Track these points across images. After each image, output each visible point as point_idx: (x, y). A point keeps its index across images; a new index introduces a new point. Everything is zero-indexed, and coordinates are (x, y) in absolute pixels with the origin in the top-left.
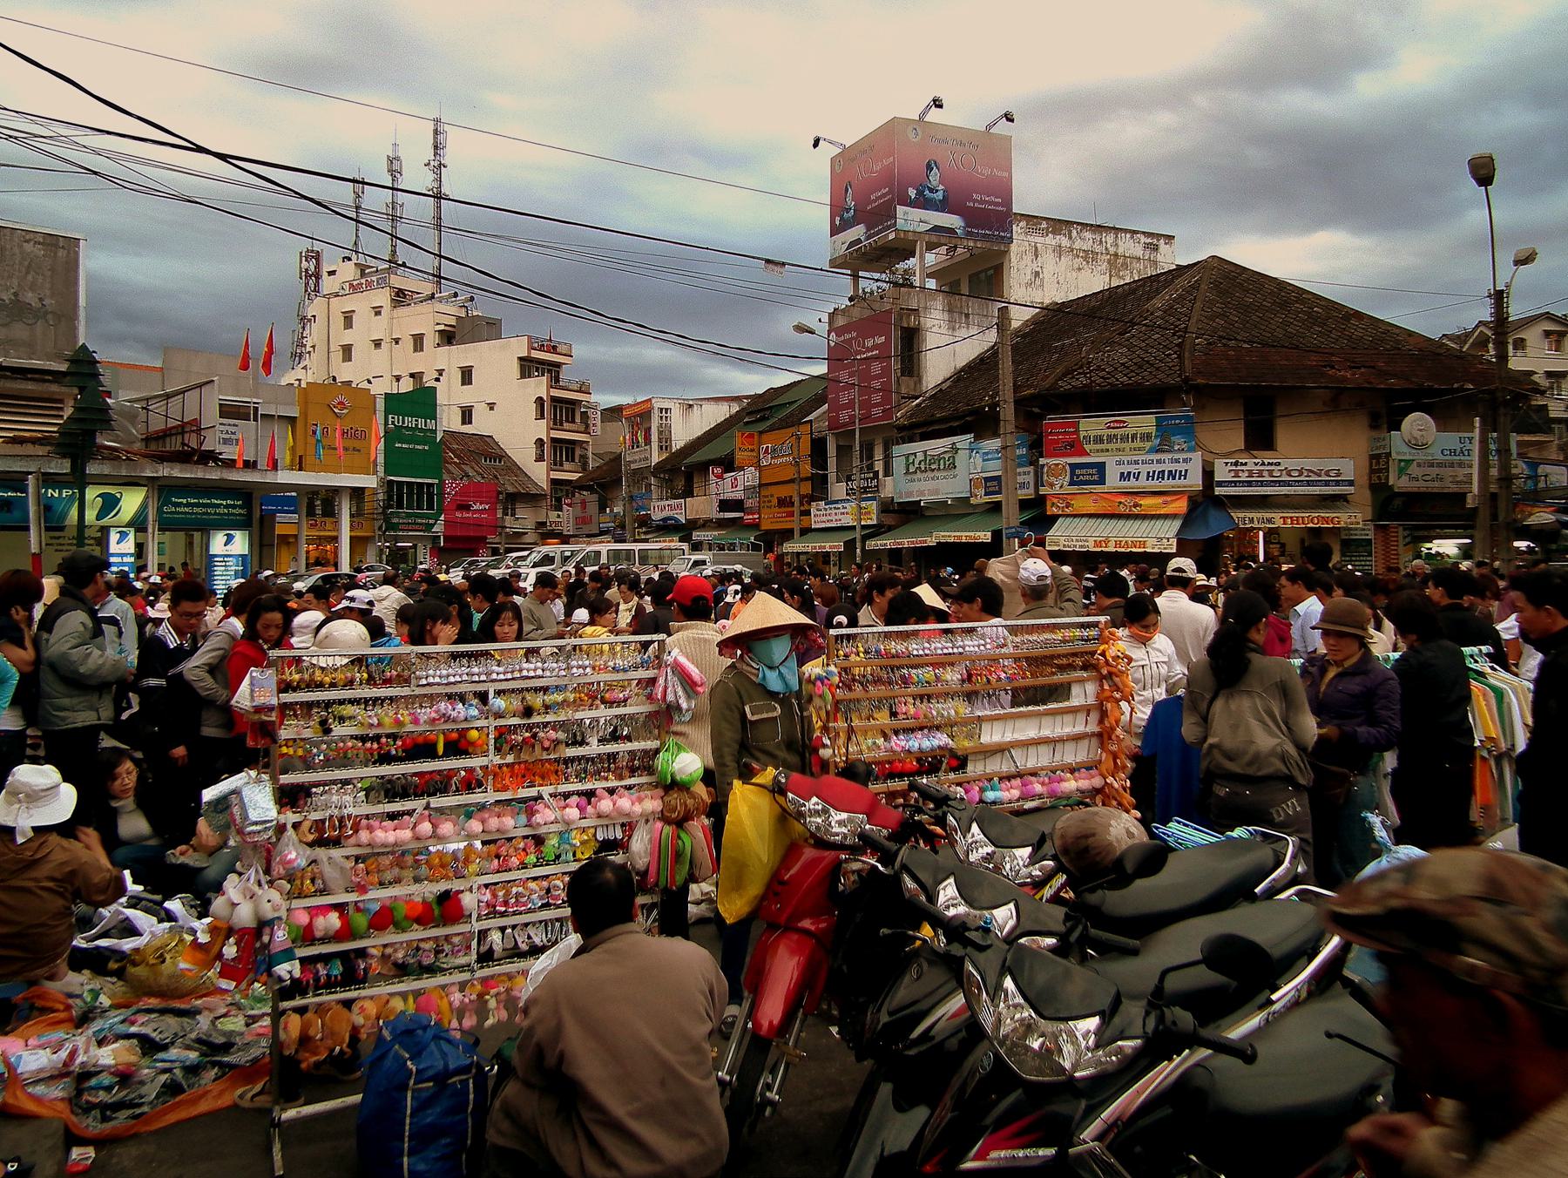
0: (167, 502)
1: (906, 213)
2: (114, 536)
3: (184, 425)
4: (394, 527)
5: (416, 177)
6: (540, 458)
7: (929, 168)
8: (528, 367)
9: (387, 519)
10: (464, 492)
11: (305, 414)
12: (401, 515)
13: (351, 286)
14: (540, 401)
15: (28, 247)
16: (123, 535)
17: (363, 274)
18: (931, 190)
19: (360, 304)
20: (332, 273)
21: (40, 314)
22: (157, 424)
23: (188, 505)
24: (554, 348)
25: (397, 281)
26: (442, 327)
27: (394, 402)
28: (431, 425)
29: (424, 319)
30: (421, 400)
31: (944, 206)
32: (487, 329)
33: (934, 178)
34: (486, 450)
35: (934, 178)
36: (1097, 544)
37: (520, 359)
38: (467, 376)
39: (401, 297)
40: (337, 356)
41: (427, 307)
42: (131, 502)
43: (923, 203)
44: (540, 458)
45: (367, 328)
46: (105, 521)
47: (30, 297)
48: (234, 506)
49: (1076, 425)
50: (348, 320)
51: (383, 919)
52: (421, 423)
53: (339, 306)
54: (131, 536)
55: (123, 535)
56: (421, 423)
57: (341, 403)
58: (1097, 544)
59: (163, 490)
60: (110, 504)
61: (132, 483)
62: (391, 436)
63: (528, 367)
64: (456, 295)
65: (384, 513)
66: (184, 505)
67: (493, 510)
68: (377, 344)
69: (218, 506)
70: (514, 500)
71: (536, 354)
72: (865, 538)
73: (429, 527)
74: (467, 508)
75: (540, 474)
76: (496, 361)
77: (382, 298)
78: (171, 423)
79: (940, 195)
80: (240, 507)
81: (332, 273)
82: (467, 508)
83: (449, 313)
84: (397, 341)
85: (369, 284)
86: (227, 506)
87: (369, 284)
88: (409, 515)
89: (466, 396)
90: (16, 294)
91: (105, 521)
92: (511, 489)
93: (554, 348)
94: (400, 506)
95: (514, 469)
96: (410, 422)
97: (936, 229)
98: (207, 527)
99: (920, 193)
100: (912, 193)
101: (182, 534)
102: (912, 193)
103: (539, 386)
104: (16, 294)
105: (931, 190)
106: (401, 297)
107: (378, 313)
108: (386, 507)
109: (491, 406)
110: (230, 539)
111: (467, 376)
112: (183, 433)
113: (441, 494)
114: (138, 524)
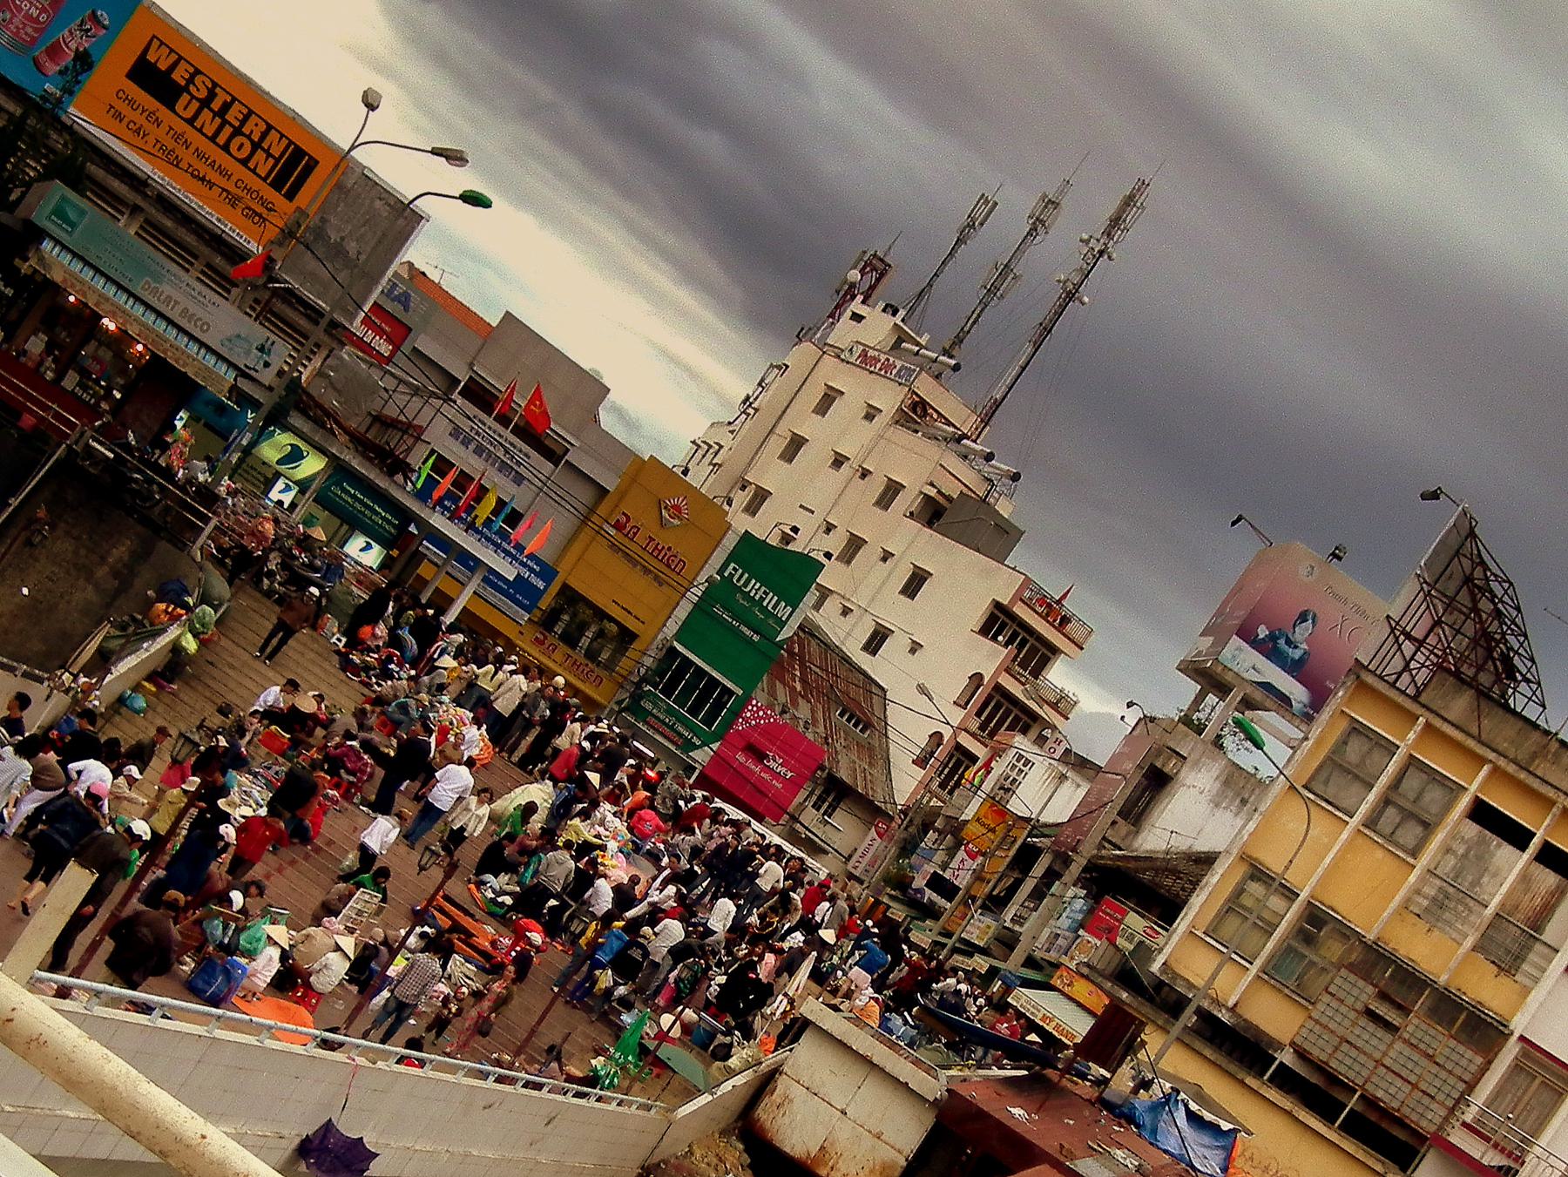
0: (339, 484)
1: (1239, 649)
2: (280, 485)
3: (410, 425)
4: (642, 714)
5: (1056, 256)
6: (921, 762)
7: (1303, 617)
8: (998, 622)
9: (637, 697)
10: (771, 732)
11: (622, 493)
12: (660, 704)
13: (864, 354)
14: (977, 679)
15: (378, 204)
16: (287, 488)
17: (896, 346)
18: (1289, 642)
19: (857, 388)
20: (857, 318)
21: (350, 264)
22: (391, 411)
23: (353, 496)
24: (1065, 620)
25: (926, 387)
26: (932, 492)
27: (750, 550)
28: (783, 611)
29: (918, 465)
30: (791, 572)
31: (1295, 668)
32: (994, 538)
33: (1302, 633)
34: (861, 706)
35: (1302, 633)
36: (1044, 1018)
37: (997, 605)
38: (915, 582)
39: (916, 414)
40: (778, 444)
41: (933, 451)
42: (312, 465)
43: (1269, 649)
44: (921, 762)
45: (840, 430)
46: (282, 468)
47: (352, 247)
48: (389, 522)
49: (1124, 913)
50: (829, 398)
51: (233, 531)
52: (770, 601)
53: (832, 373)
54: (292, 494)
55: (287, 488)
56: (770, 601)
57: (677, 508)
58: (1044, 1018)
59: (338, 470)
60: (295, 456)
61: (322, 451)
62: (720, 591)
63: (998, 622)
64: (989, 457)
65: (638, 685)
66: (349, 494)
67: (794, 785)
68: (839, 461)
69: (378, 514)
70: (836, 793)
71: (1020, 610)
72: (955, 950)
73: (689, 746)
74: (760, 756)
75: (906, 782)
76: (969, 582)
77: (889, 398)
78: (402, 418)
79: (1297, 654)
80: (394, 526)
81: (857, 318)
82: (760, 756)
83: (960, 477)
84: (865, 474)
85: (888, 367)
86: (383, 518)
87: (888, 367)
88: (670, 711)
89: (895, 612)
90: (342, 239)
91: (282, 468)
92: (844, 774)
93: (1065, 620)
94: (668, 692)
95: (878, 756)
96: (754, 588)
97: (1267, 687)
98: (353, 523)
99: (1273, 637)
100: (1263, 632)
101: (338, 522)
102: (1263, 632)
103: (990, 658)
104: (342, 239)
105: (1289, 642)
106: (916, 414)
107: (869, 417)
108: (644, 680)
109: (915, 647)
110: (368, 547)
111: (915, 582)
112: (405, 432)
113: (736, 713)
114: (303, 486)
